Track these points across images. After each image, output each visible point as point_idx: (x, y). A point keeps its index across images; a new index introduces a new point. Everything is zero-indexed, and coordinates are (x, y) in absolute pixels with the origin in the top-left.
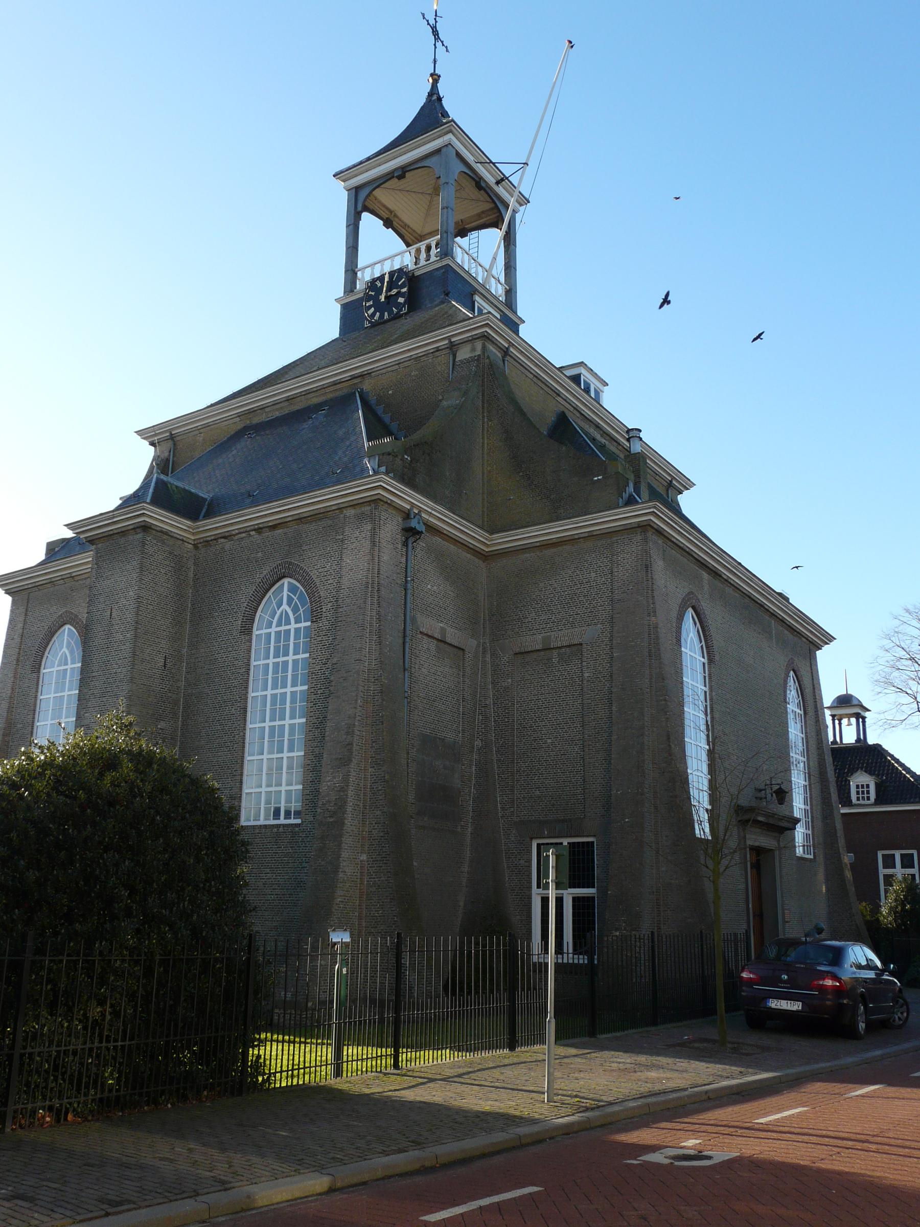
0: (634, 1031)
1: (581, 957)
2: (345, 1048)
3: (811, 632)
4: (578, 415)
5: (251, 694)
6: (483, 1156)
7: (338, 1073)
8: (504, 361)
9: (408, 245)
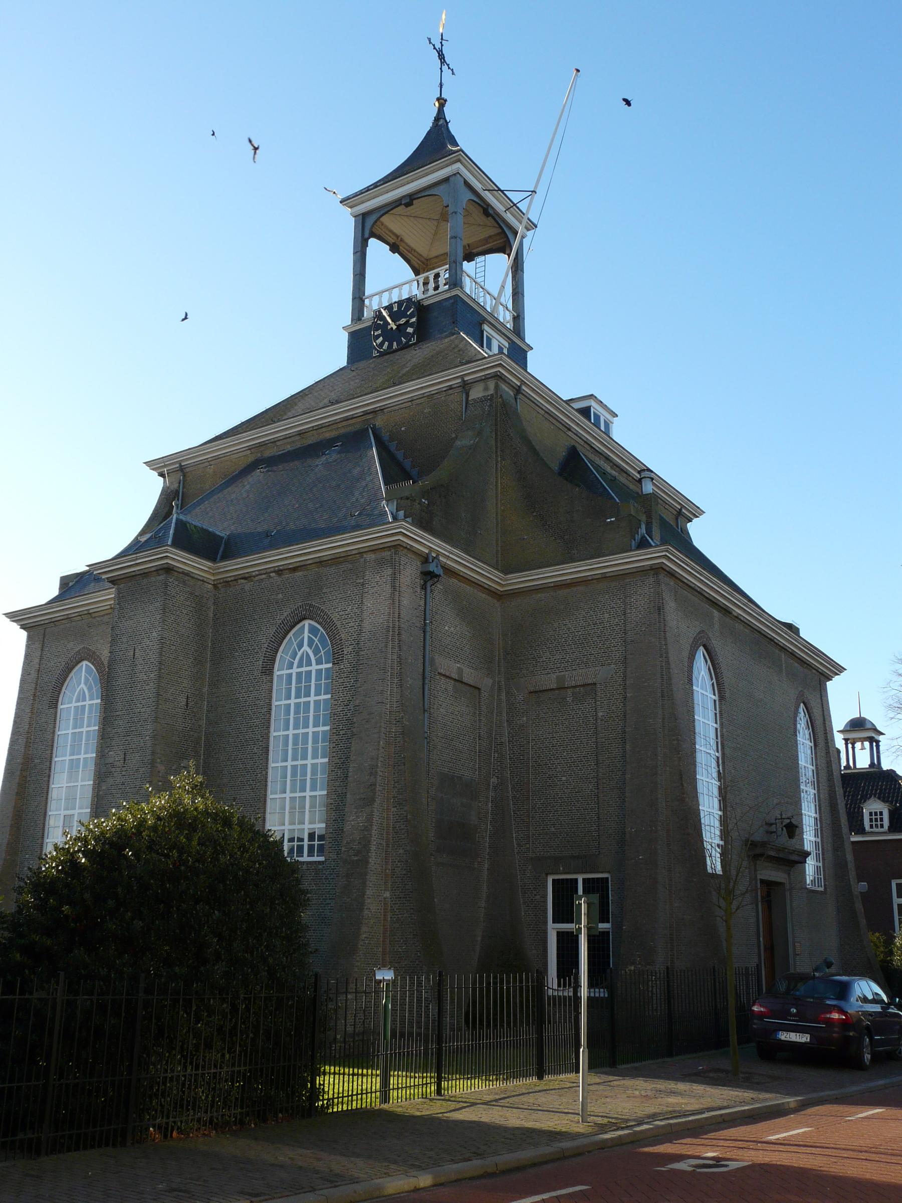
0: (651, 1062)
2: (392, 1079)
3: (821, 664)
4: (589, 448)
5: (273, 734)
6: (534, 1165)
7: (385, 1098)
8: (516, 399)
9: (417, 272)
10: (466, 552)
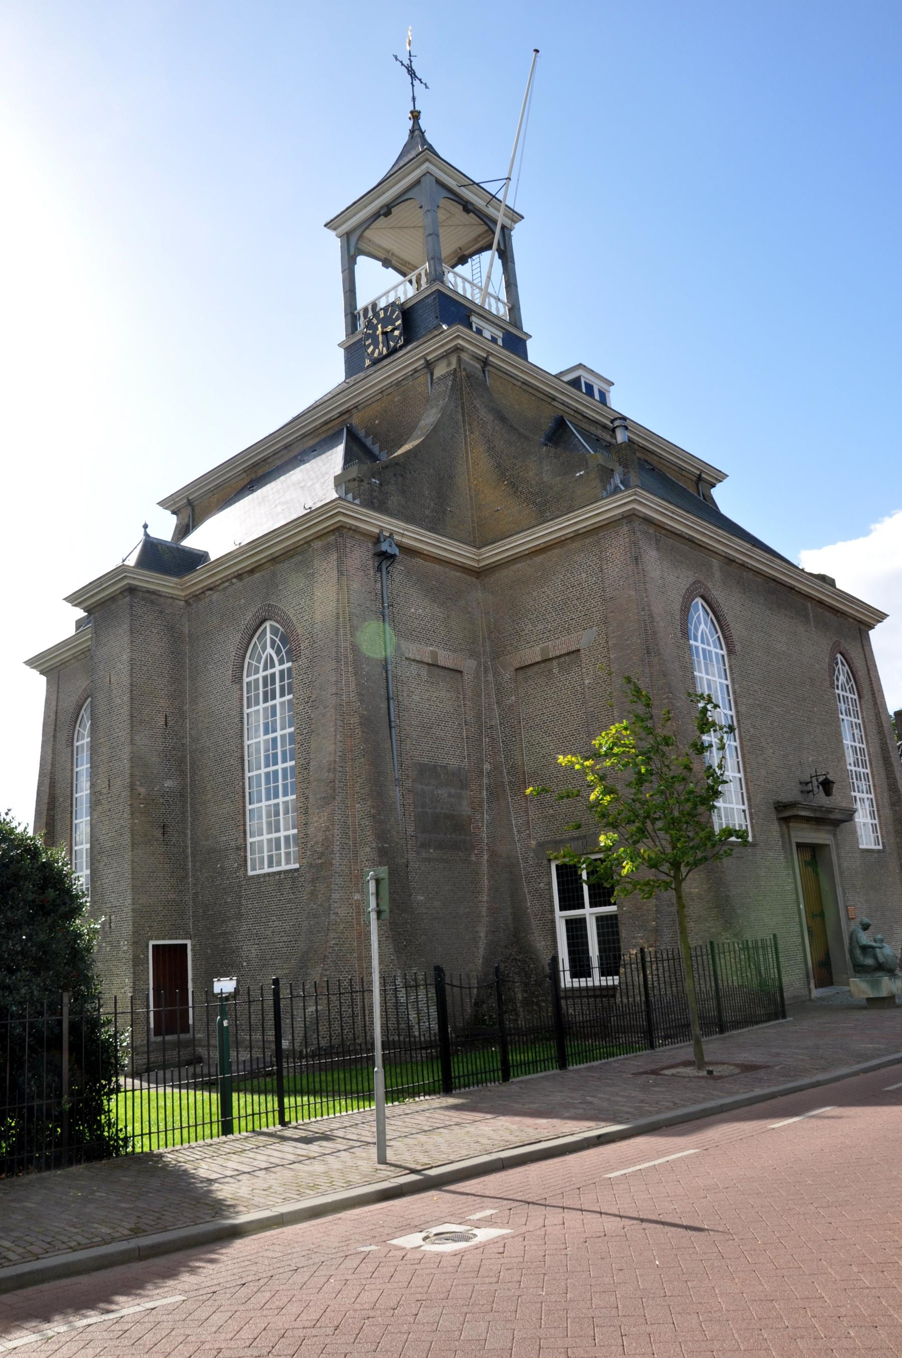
1: (610, 978)
3: (858, 611)
4: (580, 417)
8: (484, 372)
10: (432, 530)
